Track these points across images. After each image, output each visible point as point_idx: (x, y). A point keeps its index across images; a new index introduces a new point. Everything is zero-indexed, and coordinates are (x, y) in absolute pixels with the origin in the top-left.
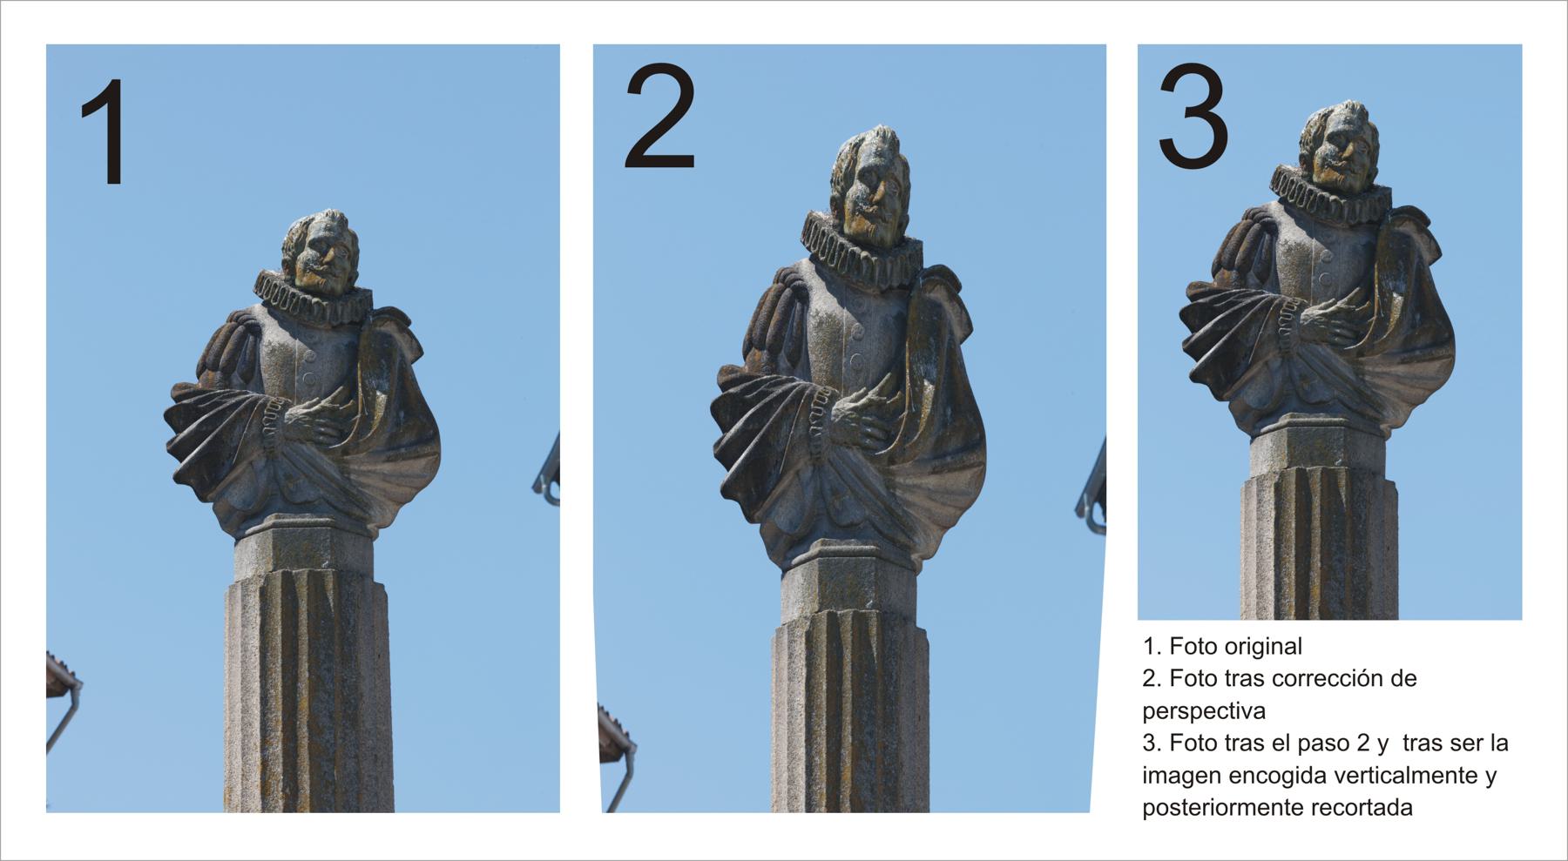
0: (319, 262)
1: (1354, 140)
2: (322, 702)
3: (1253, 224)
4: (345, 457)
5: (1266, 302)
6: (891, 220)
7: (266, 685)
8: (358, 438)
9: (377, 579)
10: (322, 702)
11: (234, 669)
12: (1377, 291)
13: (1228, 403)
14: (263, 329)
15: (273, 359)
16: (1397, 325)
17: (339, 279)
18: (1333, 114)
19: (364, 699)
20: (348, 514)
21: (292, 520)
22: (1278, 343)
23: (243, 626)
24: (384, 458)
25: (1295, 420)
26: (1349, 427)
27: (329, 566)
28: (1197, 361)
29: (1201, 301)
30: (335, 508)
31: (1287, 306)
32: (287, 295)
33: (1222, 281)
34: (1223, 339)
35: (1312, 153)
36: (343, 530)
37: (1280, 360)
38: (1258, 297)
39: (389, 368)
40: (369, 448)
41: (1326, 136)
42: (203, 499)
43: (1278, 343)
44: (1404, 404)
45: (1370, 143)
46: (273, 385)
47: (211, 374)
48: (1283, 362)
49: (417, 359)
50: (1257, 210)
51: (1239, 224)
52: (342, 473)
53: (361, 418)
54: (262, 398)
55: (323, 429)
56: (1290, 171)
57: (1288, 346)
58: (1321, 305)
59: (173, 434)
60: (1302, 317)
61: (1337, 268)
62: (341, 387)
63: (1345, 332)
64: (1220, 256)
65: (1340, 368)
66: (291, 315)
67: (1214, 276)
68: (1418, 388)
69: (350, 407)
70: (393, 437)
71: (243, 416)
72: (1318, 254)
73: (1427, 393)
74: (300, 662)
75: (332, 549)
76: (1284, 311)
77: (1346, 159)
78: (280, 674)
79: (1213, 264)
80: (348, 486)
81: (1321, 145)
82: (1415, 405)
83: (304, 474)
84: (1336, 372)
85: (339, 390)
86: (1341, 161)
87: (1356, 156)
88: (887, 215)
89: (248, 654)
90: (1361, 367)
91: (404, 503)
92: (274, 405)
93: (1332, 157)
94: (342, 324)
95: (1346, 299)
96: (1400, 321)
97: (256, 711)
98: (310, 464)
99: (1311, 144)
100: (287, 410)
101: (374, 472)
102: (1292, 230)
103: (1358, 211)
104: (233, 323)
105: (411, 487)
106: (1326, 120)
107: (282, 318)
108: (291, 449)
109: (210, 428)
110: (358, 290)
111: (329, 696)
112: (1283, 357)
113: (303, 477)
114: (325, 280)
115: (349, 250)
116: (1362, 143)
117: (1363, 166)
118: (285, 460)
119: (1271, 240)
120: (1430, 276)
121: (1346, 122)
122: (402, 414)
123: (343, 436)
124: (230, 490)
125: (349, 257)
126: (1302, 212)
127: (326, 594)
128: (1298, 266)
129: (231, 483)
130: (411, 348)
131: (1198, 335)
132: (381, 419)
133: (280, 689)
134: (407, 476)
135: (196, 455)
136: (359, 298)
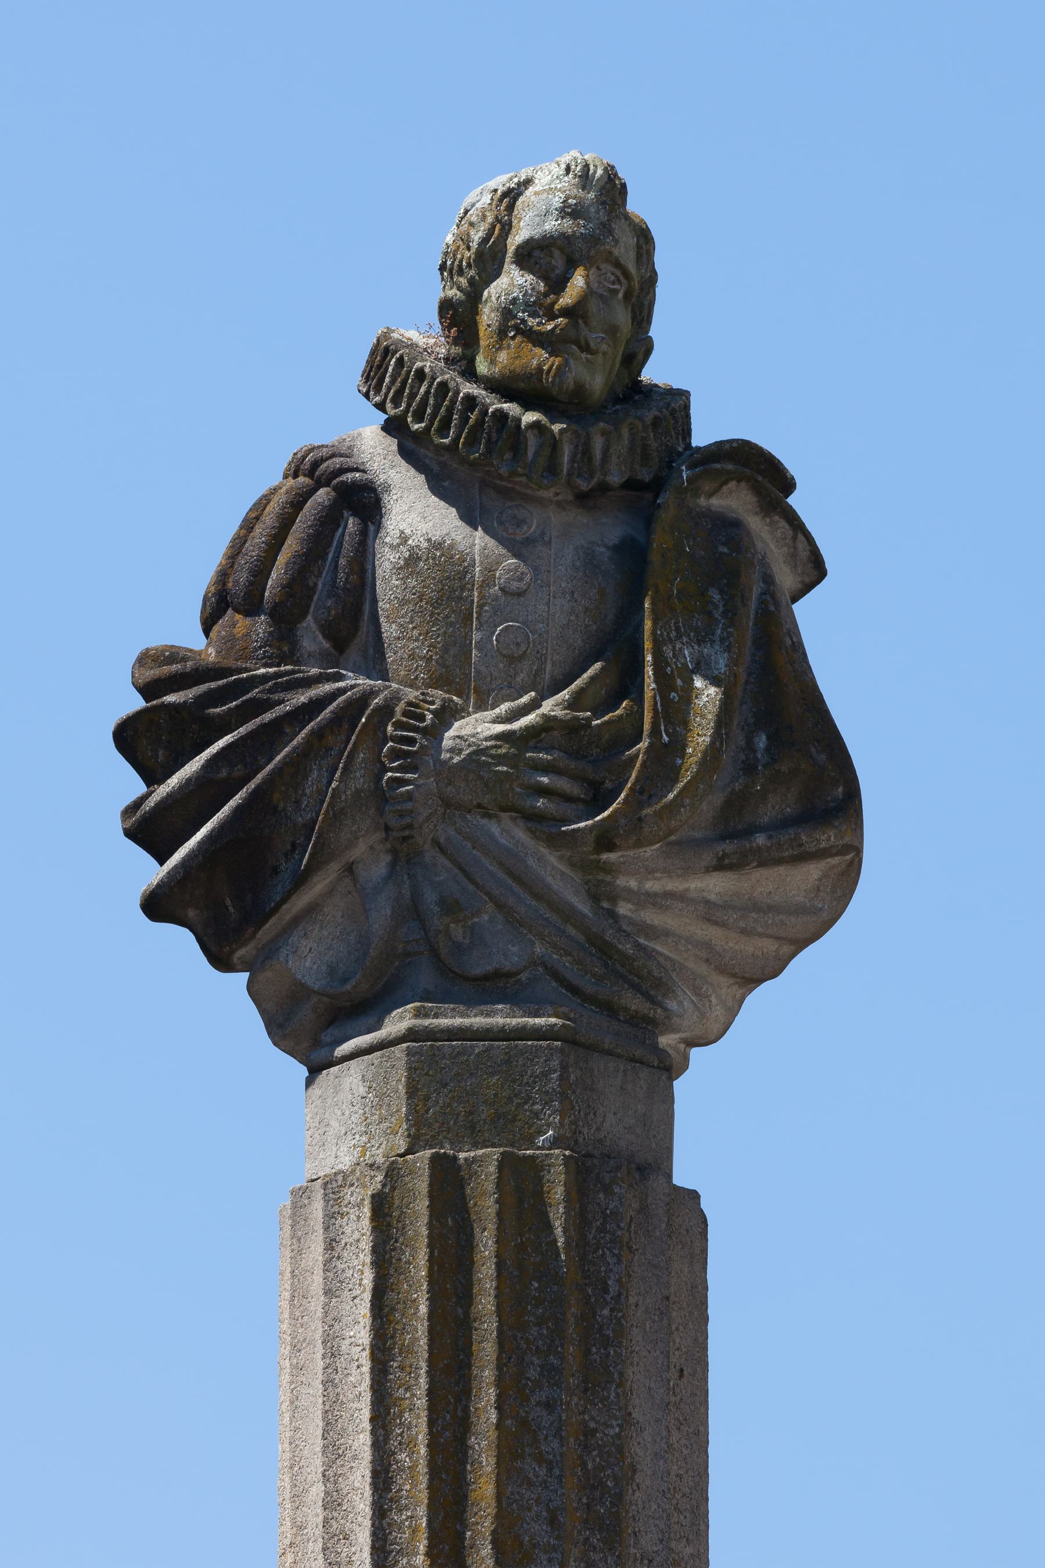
0: (543, 307)
1: (588, 262)
2: (530, 1484)
3: (315, 490)
4: (605, 856)
5: (349, 703)
6: (604, 347)
7: (387, 1439)
8: (641, 806)
9: (681, 1177)
10: (530, 1484)
11: (303, 1402)
12: (649, 671)
13: (245, 976)
14: (385, 498)
15: (412, 582)
16: (703, 763)
17: (599, 358)
18: (531, 189)
19: (638, 1478)
20: (609, 1009)
21: (458, 1021)
22: (381, 812)
23: (328, 1292)
24: (708, 858)
25: (427, 1022)
26: (575, 1043)
27: (555, 1143)
28: (162, 863)
29: (171, 698)
30: (574, 990)
31: (405, 714)
32: (453, 402)
33: (228, 644)
34: (233, 803)
35: (474, 296)
36: (593, 1048)
37: (386, 859)
38: (328, 687)
39: (731, 614)
40: (671, 832)
41: (511, 249)
42: (221, 961)
43: (381, 812)
44: (724, 980)
45: (632, 268)
46: (412, 656)
47: (242, 623)
48: (393, 865)
49: (807, 588)
50: (324, 452)
51: (274, 491)
52: (595, 898)
53: (648, 750)
54: (382, 690)
55: (545, 780)
56: (413, 346)
57: (408, 820)
58: (497, 711)
59: (139, 787)
60: (447, 742)
61: (542, 607)
62: (598, 665)
63: (563, 784)
64: (223, 575)
65: (549, 879)
66: (464, 461)
67: (207, 631)
68: (760, 935)
69: (620, 717)
70: (735, 804)
71: (330, 739)
72: (489, 571)
73: (786, 949)
74: (474, 1384)
75: (563, 1096)
76: (399, 725)
77: (566, 312)
78: (424, 1414)
79: (206, 599)
80: (609, 935)
81: (498, 275)
82: (753, 981)
83: (492, 898)
84: (539, 893)
85: (590, 672)
86: (552, 317)
87: (593, 306)
88: (594, 337)
89: (341, 1363)
90: (608, 878)
91: (759, 981)
92: (413, 712)
93: (528, 306)
94: (603, 488)
95: (565, 694)
96: (712, 754)
97: (362, 1504)
98: (510, 874)
99: (472, 272)
100: (449, 726)
101: (680, 897)
102: (419, 506)
103: (598, 454)
104: (301, 479)
105: (778, 938)
106: (511, 208)
107: (436, 468)
108: (459, 832)
109: (239, 771)
110: (651, 391)
111: (550, 1469)
112: (394, 852)
113: (490, 907)
114: (557, 361)
115: (626, 274)
116: (610, 268)
117: (612, 331)
118: (442, 860)
119: (364, 533)
120: (794, 631)
121: (568, 211)
122: (761, 741)
123: (599, 800)
124: (293, 939)
125: (627, 296)
126: (446, 457)
127: (546, 1215)
128: (436, 604)
129: (296, 921)
130: (793, 557)
131: (163, 790)
132: (705, 753)
133: (423, 1450)
134: (771, 909)
135: (201, 843)
136: (654, 412)
